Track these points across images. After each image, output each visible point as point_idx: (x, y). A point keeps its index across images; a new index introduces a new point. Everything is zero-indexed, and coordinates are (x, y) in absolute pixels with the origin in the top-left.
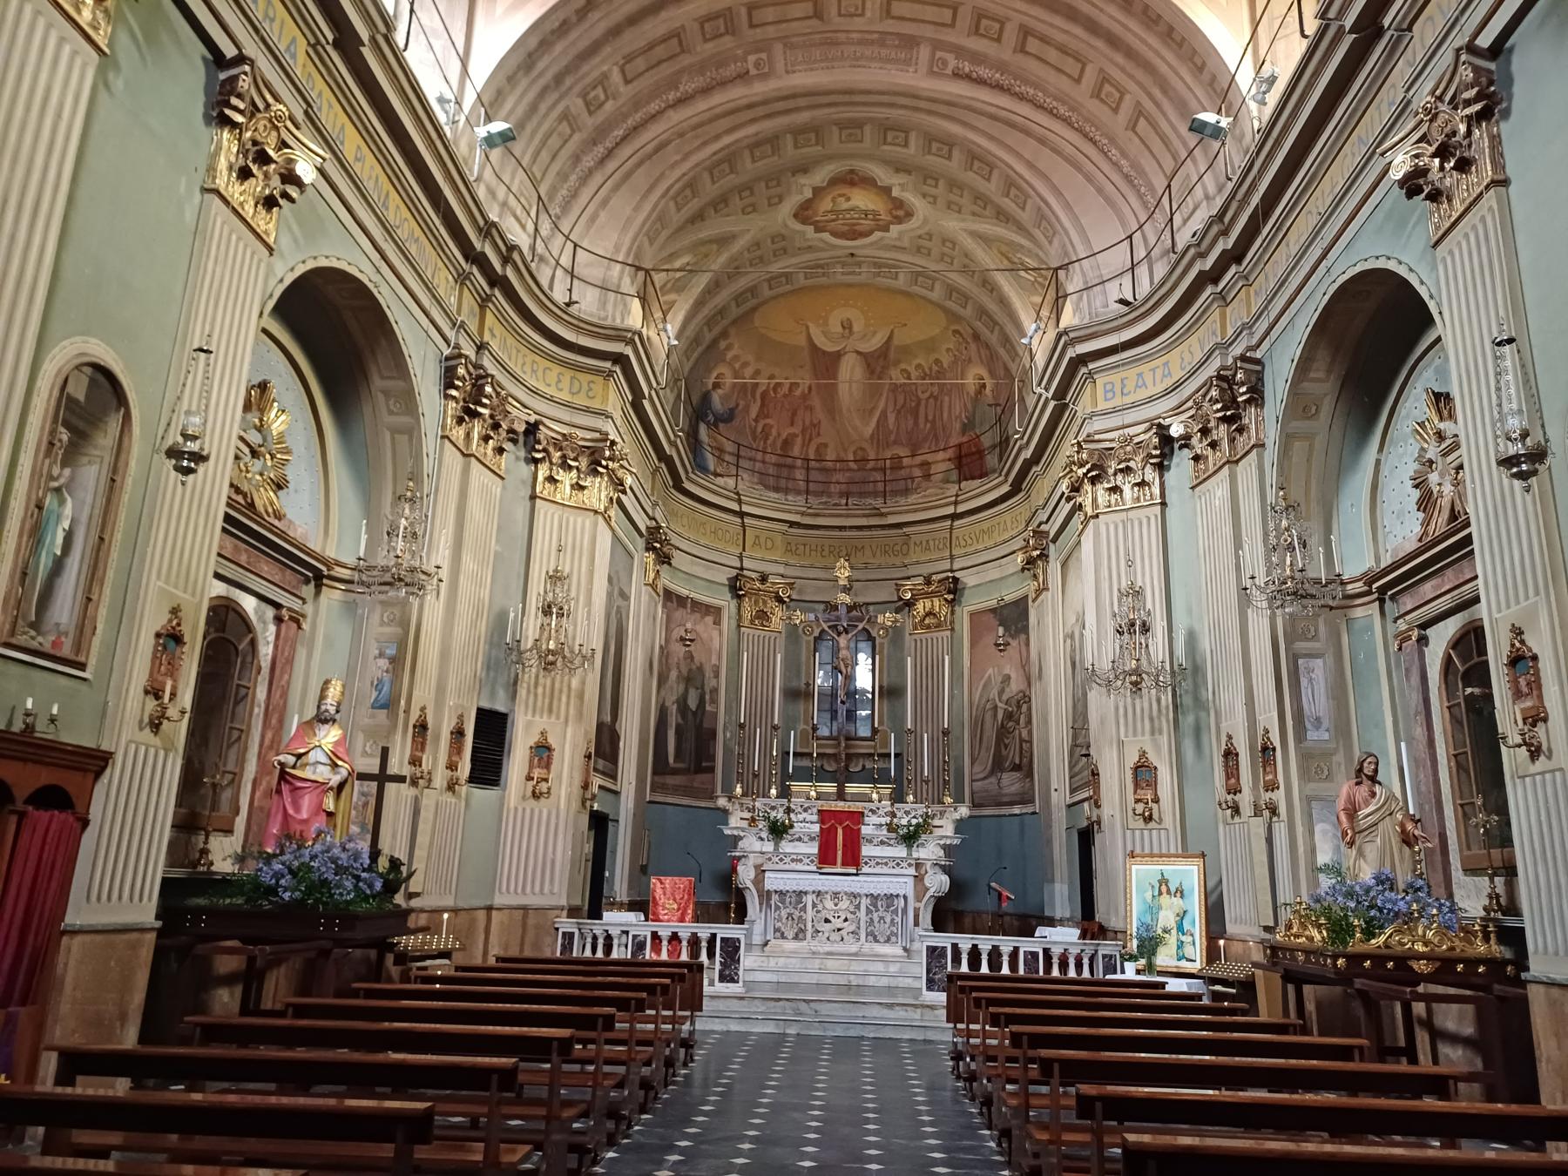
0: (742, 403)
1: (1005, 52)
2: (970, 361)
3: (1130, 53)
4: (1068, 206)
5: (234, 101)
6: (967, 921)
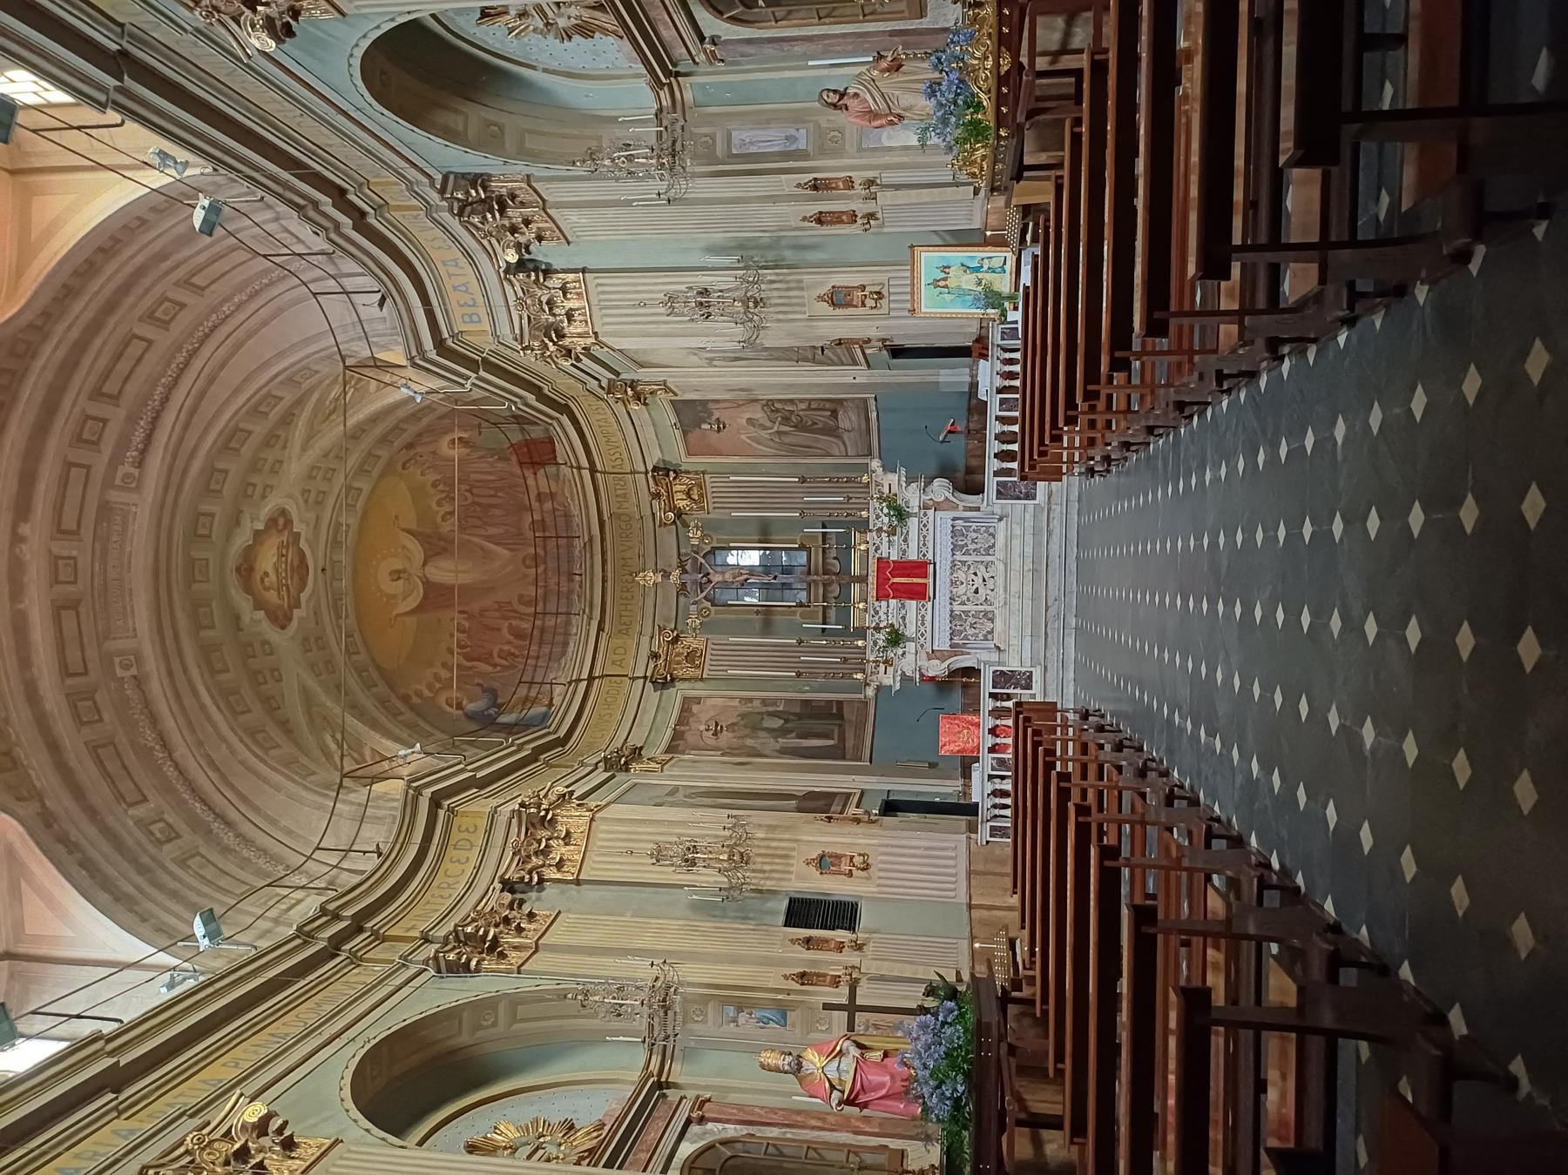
0: (477, 680)
2: (434, 453)
3: (125, 289)
4: (281, 355)
6: (974, 462)
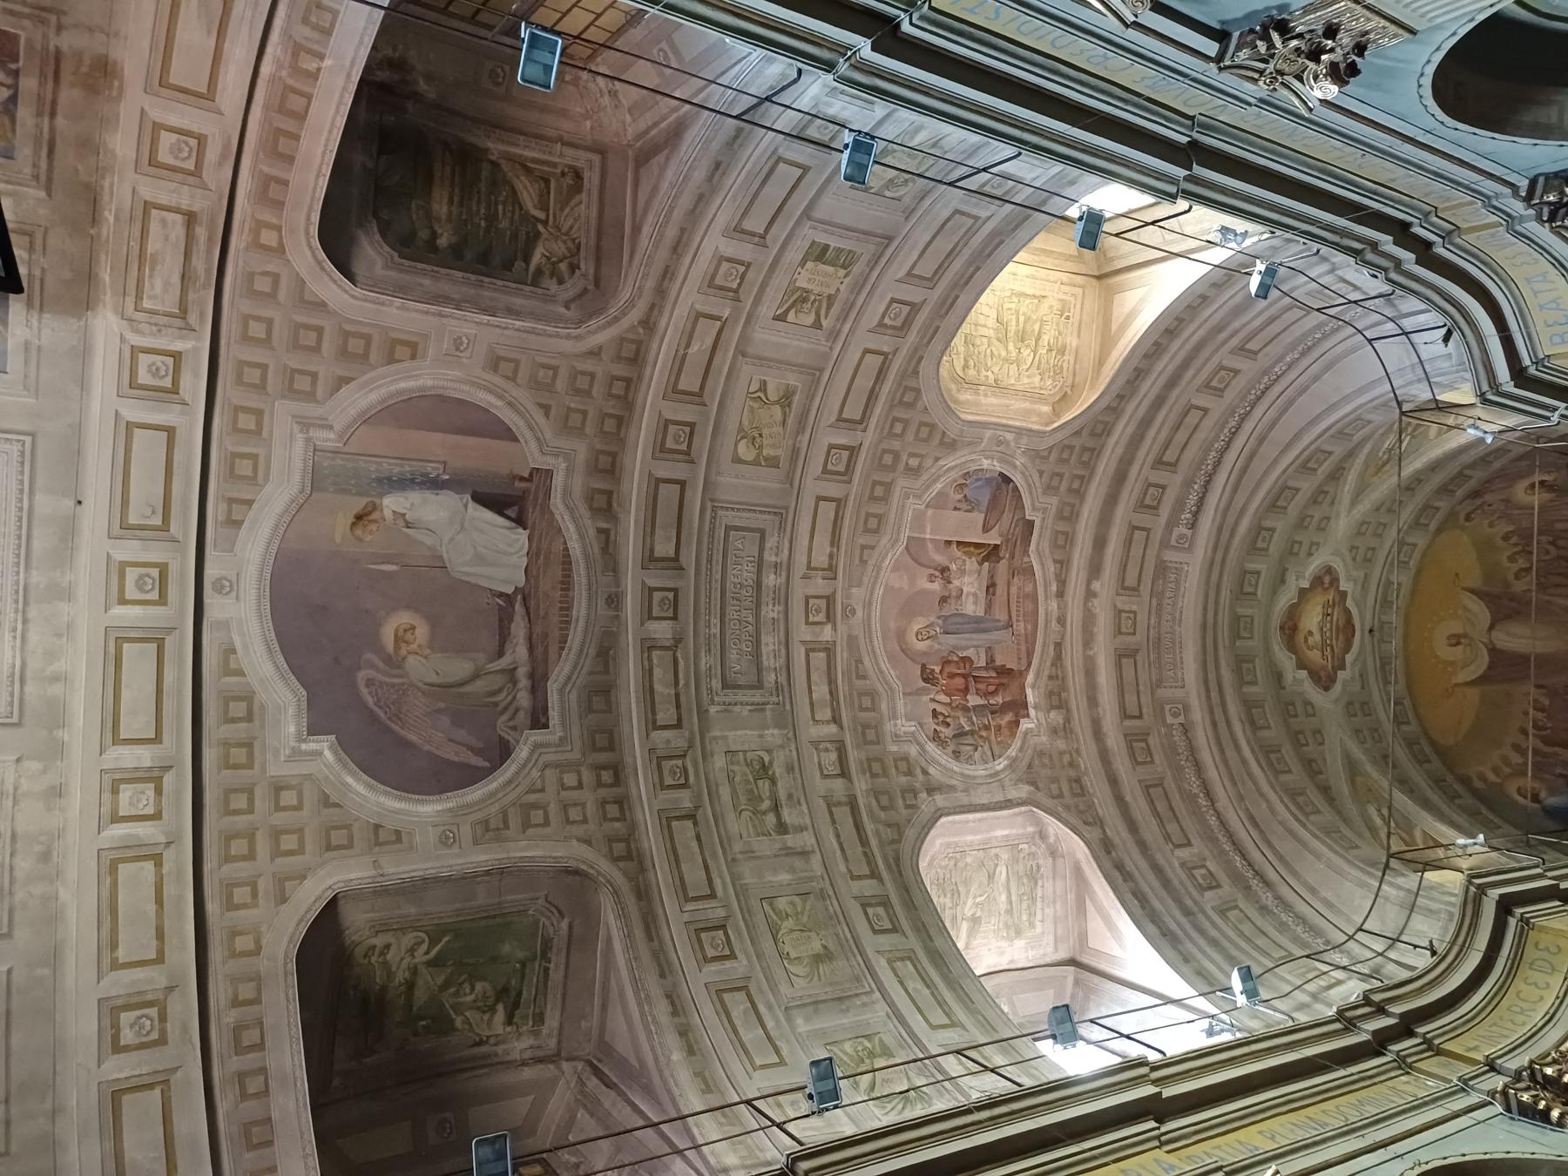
0: (1559, 771)
1: (1175, 481)
2: (1507, 501)
3: (1185, 365)
4: (1333, 407)
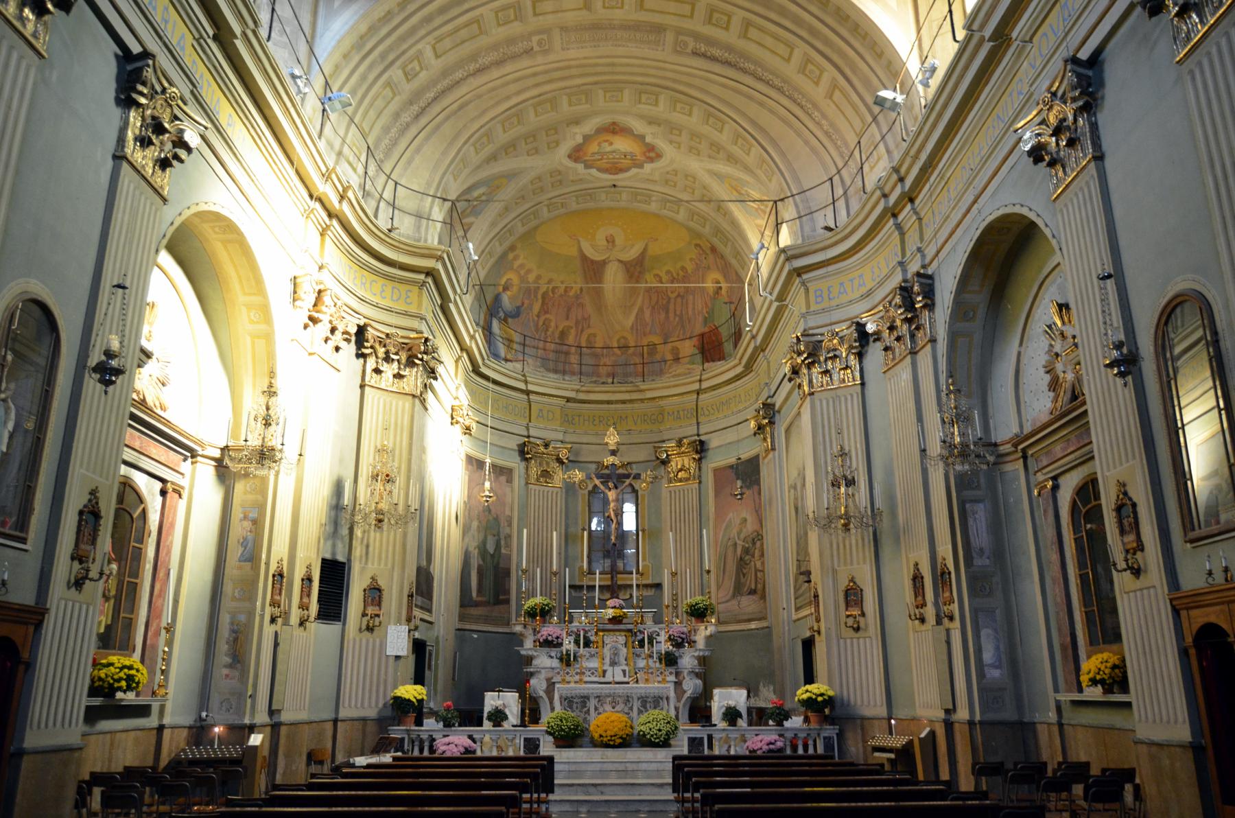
0: (526, 302)
2: (709, 268)
5: (140, 88)
